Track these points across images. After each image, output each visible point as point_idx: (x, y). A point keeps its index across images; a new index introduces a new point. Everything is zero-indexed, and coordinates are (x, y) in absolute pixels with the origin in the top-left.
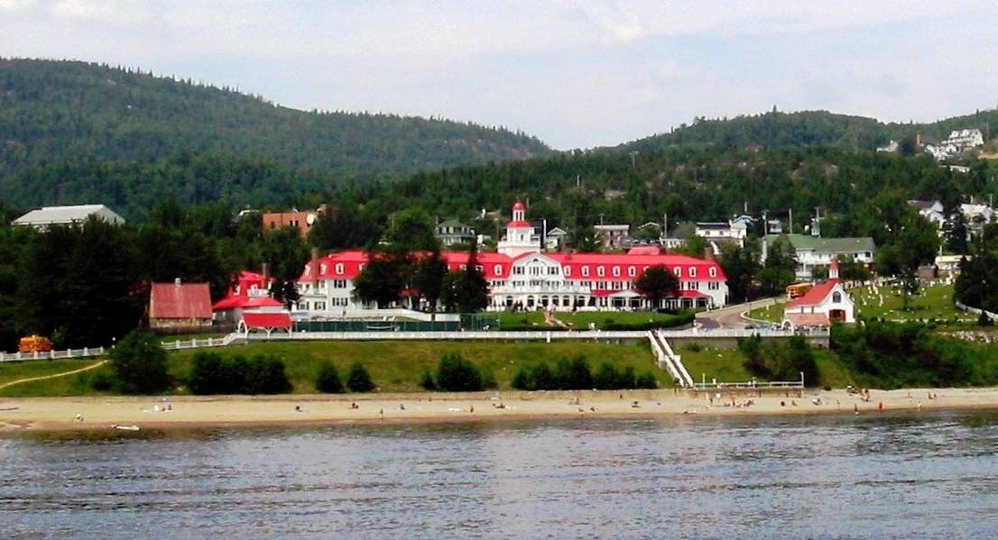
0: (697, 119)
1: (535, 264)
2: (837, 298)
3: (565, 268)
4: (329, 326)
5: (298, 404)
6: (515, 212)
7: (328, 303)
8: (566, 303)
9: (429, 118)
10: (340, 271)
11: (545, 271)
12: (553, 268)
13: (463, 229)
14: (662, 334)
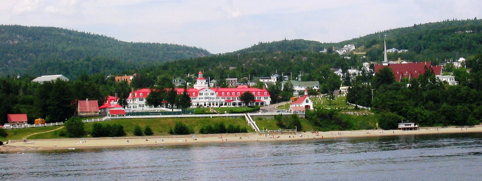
1: (206, 92)
2: (307, 101)
4: (138, 114)
6: (199, 75)
7: (138, 106)
8: (217, 105)
9: (170, 44)
11: (210, 94)
14: (249, 114)
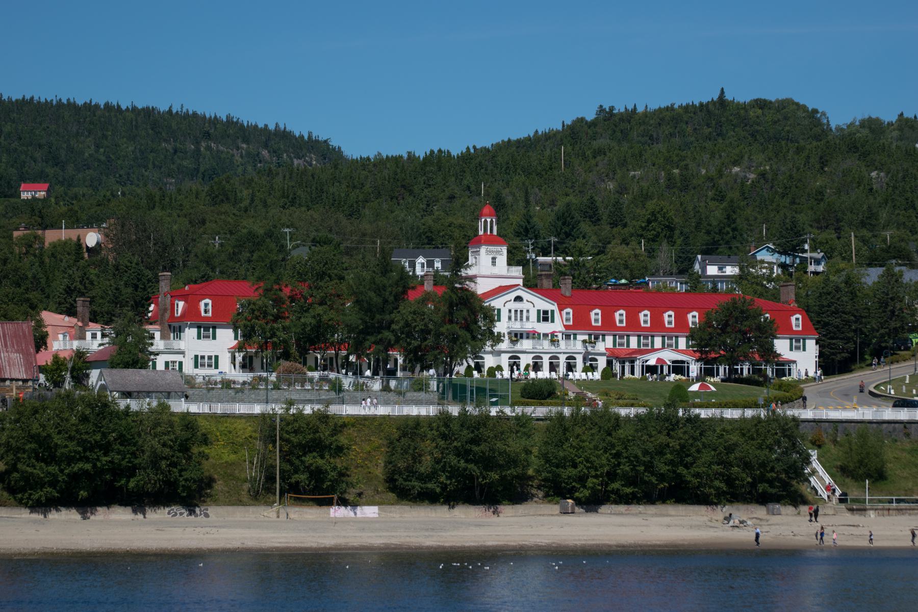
5: (278, 519)
9: (167, 109)
10: (206, 312)
11: (533, 316)
12: (546, 312)
13: (101, 301)
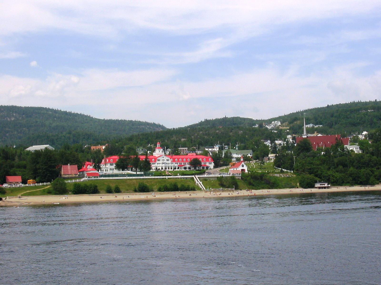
0: (205, 119)
1: (163, 159)
2: (243, 166)
3: (171, 159)
6: (157, 145)
7: (109, 170)
8: (171, 169)
11: (166, 160)
14: (197, 176)
